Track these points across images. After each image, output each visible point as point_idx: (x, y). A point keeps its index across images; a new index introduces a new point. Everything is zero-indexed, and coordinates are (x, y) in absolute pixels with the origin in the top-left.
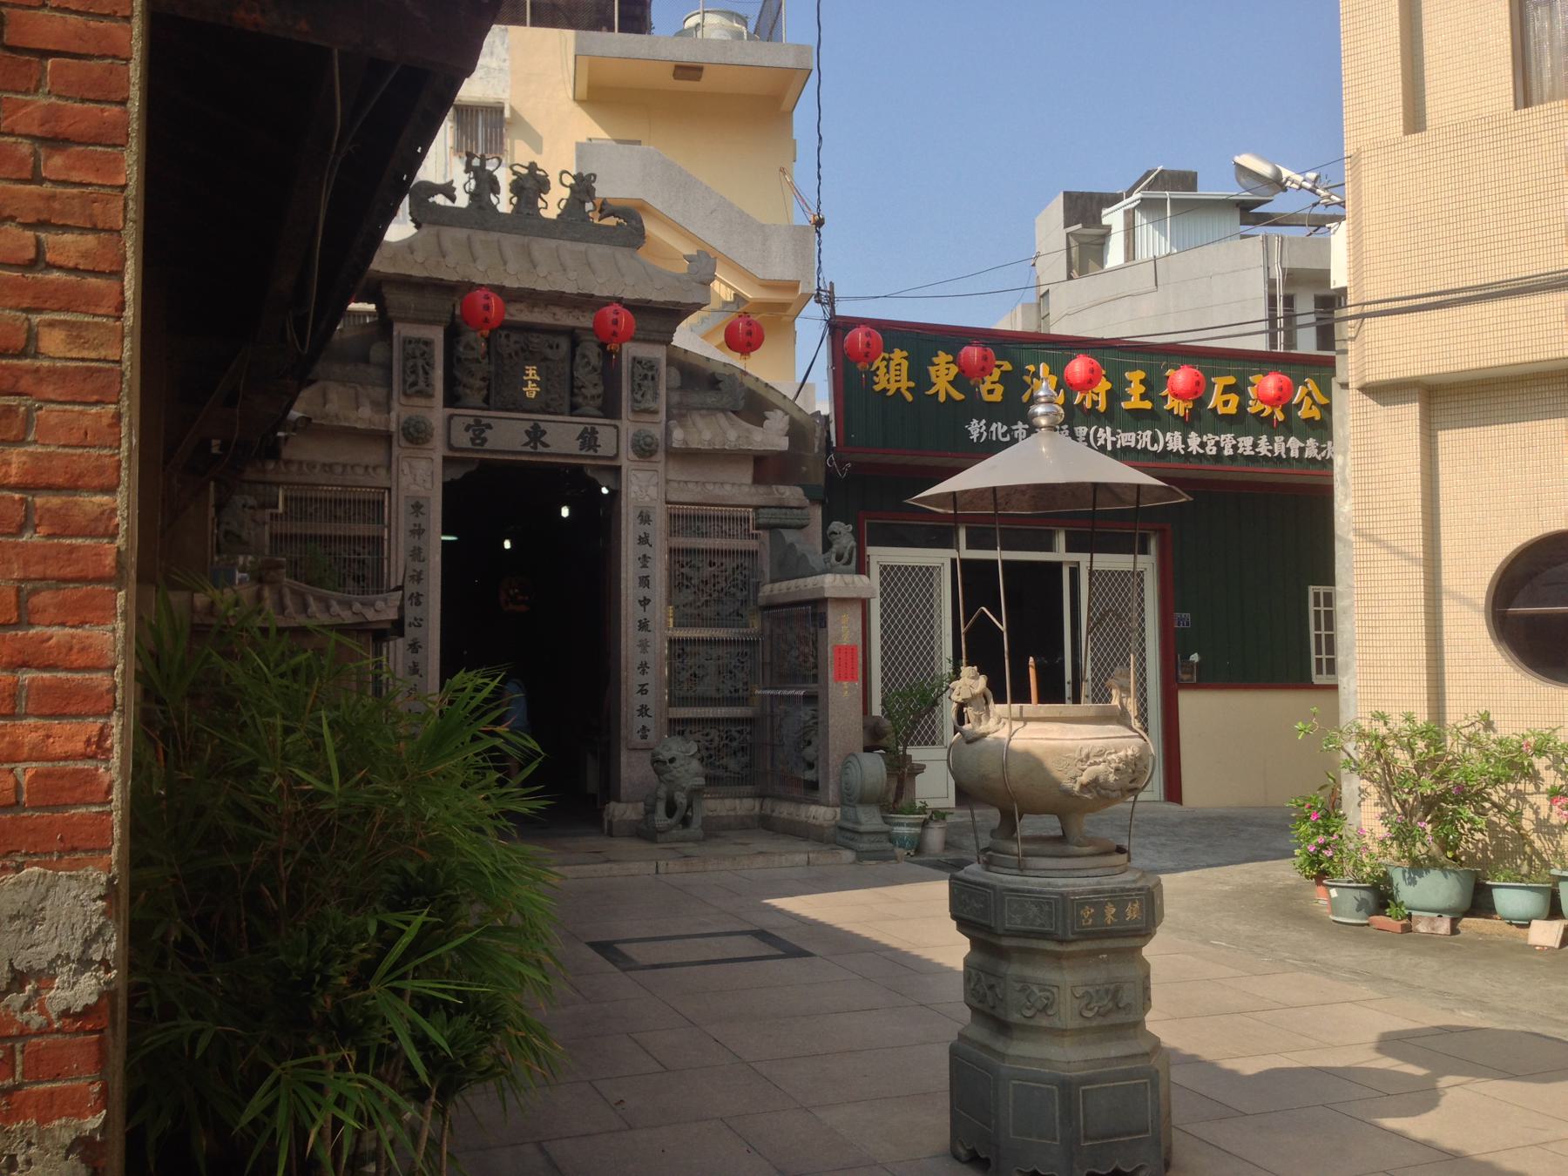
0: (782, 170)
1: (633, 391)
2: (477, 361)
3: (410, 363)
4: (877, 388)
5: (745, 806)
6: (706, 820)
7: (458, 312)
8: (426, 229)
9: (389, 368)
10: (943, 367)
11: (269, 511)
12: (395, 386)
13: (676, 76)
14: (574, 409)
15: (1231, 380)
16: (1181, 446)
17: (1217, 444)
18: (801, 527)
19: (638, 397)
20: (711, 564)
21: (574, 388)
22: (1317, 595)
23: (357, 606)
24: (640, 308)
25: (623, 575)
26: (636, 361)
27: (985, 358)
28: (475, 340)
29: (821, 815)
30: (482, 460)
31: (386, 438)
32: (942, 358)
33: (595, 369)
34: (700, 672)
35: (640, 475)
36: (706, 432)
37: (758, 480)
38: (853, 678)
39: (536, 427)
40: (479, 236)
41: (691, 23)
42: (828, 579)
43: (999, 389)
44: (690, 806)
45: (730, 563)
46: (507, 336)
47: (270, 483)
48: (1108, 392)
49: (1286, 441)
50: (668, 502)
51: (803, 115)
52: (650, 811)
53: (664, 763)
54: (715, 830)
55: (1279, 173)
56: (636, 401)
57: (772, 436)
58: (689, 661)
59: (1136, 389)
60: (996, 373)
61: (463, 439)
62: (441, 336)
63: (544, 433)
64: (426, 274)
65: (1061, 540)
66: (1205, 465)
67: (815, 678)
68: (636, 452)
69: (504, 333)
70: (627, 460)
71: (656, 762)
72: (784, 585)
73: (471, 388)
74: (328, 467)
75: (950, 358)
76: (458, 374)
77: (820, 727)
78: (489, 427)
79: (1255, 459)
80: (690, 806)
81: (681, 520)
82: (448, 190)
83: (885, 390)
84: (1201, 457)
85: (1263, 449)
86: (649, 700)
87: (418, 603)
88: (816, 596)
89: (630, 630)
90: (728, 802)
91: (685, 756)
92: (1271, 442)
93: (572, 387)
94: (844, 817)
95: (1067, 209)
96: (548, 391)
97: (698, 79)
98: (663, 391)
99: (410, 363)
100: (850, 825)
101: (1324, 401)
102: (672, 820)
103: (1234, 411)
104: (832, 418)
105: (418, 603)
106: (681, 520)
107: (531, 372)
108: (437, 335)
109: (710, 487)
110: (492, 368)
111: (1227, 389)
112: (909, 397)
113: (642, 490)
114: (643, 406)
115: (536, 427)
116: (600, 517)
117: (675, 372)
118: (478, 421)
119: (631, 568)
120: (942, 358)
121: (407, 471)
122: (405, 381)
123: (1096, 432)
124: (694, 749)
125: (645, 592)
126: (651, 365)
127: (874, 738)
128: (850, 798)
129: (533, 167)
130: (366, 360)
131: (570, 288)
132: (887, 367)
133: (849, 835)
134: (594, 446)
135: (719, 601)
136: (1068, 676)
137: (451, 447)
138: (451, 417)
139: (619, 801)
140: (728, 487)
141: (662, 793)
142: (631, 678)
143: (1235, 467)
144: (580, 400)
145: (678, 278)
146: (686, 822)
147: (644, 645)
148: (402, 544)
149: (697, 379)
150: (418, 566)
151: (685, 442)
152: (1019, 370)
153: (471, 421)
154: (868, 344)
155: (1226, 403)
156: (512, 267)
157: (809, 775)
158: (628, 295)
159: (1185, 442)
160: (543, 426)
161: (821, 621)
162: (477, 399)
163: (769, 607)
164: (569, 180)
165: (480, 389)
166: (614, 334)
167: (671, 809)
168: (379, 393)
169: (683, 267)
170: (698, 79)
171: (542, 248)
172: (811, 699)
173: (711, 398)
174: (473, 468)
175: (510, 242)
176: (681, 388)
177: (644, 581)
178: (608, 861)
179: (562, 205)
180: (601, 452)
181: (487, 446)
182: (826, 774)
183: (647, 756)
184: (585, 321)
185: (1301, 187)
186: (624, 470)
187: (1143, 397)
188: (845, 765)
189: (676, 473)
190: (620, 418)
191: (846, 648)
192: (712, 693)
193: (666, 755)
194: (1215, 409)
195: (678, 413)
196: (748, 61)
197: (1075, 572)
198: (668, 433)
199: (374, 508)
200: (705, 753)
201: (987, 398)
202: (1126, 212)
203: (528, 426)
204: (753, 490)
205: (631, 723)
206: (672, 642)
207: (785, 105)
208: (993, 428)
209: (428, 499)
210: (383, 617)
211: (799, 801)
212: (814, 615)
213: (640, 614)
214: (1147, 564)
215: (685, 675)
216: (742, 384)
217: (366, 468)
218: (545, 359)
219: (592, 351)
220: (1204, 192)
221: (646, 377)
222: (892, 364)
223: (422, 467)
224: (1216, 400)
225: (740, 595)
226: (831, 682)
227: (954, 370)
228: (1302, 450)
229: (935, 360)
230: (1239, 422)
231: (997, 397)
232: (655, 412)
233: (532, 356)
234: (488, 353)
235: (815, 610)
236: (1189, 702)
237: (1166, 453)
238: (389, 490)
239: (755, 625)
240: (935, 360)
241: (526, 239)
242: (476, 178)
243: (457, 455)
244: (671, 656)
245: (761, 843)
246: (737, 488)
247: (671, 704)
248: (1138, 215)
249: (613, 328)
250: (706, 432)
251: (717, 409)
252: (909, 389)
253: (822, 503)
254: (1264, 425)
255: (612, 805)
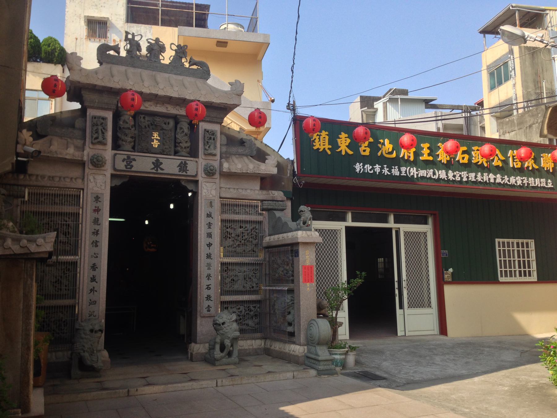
0: (258, 81)
1: (204, 145)
2: (129, 129)
3: (95, 128)
4: (315, 148)
5: (257, 344)
6: (239, 351)
7: (119, 105)
8: (104, 65)
9: (84, 131)
10: (343, 139)
11: (20, 199)
12: (87, 139)
13: (217, 45)
14: (176, 153)
15: (465, 148)
16: (445, 177)
17: (460, 176)
18: (282, 210)
19: (207, 148)
20: (241, 227)
21: (176, 143)
22: (499, 243)
23: (24, 242)
24: (209, 106)
25: (199, 232)
26: (206, 131)
27: (366, 133)
28: (128, 116)
29: (298, 350)
30: (131, 176)
31: (82, 164)
32: (343, 135)
33: (186, 135)
34: (235, 279)
35: (207, 184)
36: (241, 164)
37: (262, 188)
38: (312, 281)
39: (157, 160)
40: (131, 70)
41: (223, 27)
42: (300, 233)
43: (368, 150)
44: (232, 346)
45: (249, 227)
46: (144, 118)
47: (21, 186)
48: (414, 152)
49: (488, 175)
50: (220, 198)
51: (265, 62)
52: (212, 348)
53: (220, 325)
54: (244, 357)
55: (524, 34)
56: (205, 149)
57: (269, 168)
58: (231, 273)
59: (426, 151)
60: (367, 143)
61: (121, 166)
62: (111, 116)
63: (161, 163)
64: (103, 84)
65: (391, 218)
66: (456, 185)
67: (293, 281)
68: (206, 174)
69: (142, 116)
70: (201, 177)
71: (215, 324)
72: (276, 237)
73: (126, 141)
74: (52, 178)
75: (347, 135)
76: (119, 135)
77: (296, 305)
78: (134, 160)
79: (476, 182)
80: (232, 346)
81: (227, 206)
82: (116, 49)
83: (318, 149)
84: (454, 181)
85: (479, 179)
86: (211, 292)
87: (97, 246)
88: (294, 242)
89: (202, 258)
90: (249, 342)
91: (229, 321)
92: (482, 175)
93: (175, 142)
94: (309, 351)
95: (361, 102)
96: (164, 144)
97: (226, 47)
98: (218, 145)
99: (95, 128)
100: (313, 356)
101: (503, 158)
102: (223, 353)
103: (467, 162)
104: (295, 161)
105: (97, 246)
106: (227, 206)
107: (156, 135)
108: (109, 115)
109: (240, 191)
110: (136, 132)
111: (464, 152)
112: (329, 152)
113: (208, 192)
114: (209, 152)
115: (157, 160)
116: (188, 209)
117: (224, 138)
118: (129, 157)
119: (203, 228)
120: (343, 135)
121: (92, 180)
122: (92, 137)
123: (410, 169)
124: (234, 317)
125: (209, 240)
126: (213, 133)
127: (321, 311)
128: (311, 342)
129: (157, 40)
130: (73, 126)
131: (175, 95)
132: (319, 138)
133: (313, 361)
134: (186, 171)
135: (244, 244)
136: (396, 279)
137: (115, 169)
138: (115, 155)
139: (196, 343)
140: (249, 191)
141: (218, 340)
142: (202, 282)
143: (468, 186)
144: (179, 149)
145: (226, 92)
146: (230, 354)
147: (209, 266)
148: (89, 216)
149: (236, 142)
150: (97, 227)
151: (229, 169)
152: (377, 142)
153: (126, 157)
154: (314, 125)
155: (463, 158)
156: (146, 84)
157: (290, 329)
158: (202, 99)
159: (447, 175)
160: (161, 160)
161: (296, 254)
162: (129, 147)
163: (268, 247)
164: (174, 48)
165: (130, 142)
166: (196, 115)
167: (222, 348)
168: (79, 142)
169: (228, 88)
170: (226, 47)
171: (161, 77)
172: (291, 291)
173: (241, 150)
174: (126, 180)
175: (146, 73)
176: (227, 145)
177: (209, 235)
178: (192, 380)
179: (171, 59)
180: (189, 173)
181: (133, 169)
182: (299, 330)
183: (210, 321)
184: (182, 112)
185: (535, 40)
186: (200, 182)
187: (429, 155)
188: (310, 324)
189: (225, 184)
190: (198, 157)
191: (308, 267)
192: (241, 288)
193: (221, 321)
194: (459, 161)
195: (225, 156)
196: (245, 39)
197: (398, 233)
198: (221, 165)
199: (75, 199)
200: (238, 318)
201: (363, 153)
202: (384, 103)
203: (154, 160)
204: (260, 192)
205: (202, 304)
206: (222, 264)
207: (259, 58)
208: (366, 167)
209: (102, 194)
210: (43, 249)
211: (285, 342)
212: (292, 251)
213: (207, 251)
214: (427, 229)
215: (228, 280)
216: (255, 144)
217: (72, 179)
218: (162, 129)
219: (184, 126)
220: (411, 96)
221: (210, 138)
222: (321, 137)
223: (100, 178)
224: (459, 157)
225: (255, 242)
226: (301, 283)
227: (349, 141)
228: (495, 179)
229: (340, 136)
230: (469, 166)
231: (367, 153)
232: (215, 155)
233: (155, 127)
234: (135, 125)
235: (293, 248)
236: (449, 290)
237: (439, 180)
238: (83, 189)
239: (261, 256)
240: (340, 136)
241: (154, 73)
242: (130, 44)
243: (118, 173)
244: (222, 271)
245: (268, 366)
246: (252, 192)
247: (221, 294)
248: (388, 104)
249: (194, 112)
250: (241, 164)
251: (243, 155)
252: (329, 149)
253: (291, 199)
254: (480, 168)
255: (193, 344)
